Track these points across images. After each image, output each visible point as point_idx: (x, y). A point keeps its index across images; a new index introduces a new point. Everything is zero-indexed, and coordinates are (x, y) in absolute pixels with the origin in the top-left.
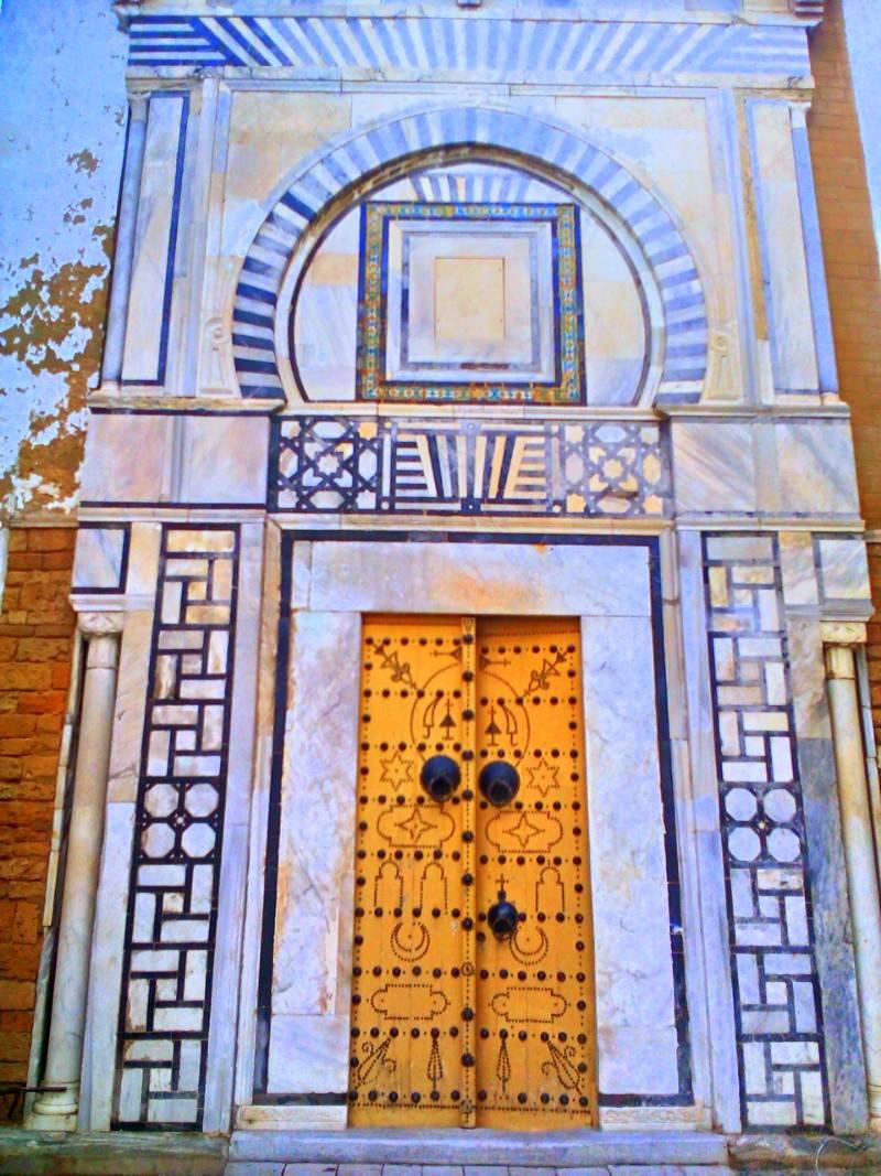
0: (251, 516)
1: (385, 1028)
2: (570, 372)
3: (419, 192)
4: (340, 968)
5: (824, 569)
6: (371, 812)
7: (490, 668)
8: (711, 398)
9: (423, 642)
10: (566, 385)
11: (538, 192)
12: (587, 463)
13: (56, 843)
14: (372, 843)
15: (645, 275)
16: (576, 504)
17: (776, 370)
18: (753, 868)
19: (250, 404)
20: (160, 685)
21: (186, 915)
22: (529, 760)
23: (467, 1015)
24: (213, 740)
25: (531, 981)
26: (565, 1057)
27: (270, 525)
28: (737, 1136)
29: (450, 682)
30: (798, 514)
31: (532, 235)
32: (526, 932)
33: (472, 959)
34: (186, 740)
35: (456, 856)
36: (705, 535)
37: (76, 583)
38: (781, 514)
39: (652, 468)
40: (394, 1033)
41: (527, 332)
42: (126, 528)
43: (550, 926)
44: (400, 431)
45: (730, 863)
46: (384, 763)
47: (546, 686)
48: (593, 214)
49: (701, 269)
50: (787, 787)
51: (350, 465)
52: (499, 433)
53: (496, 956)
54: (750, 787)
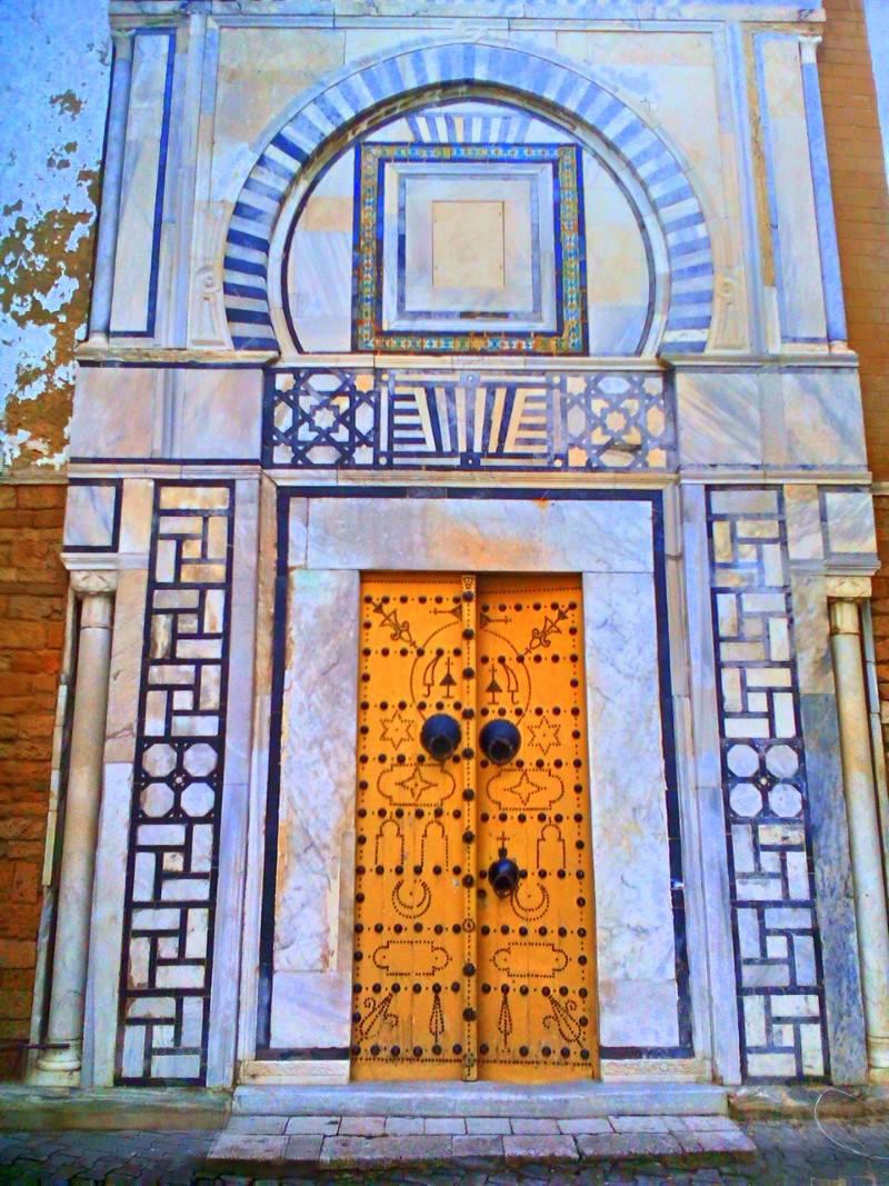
0: (245, 472)
1: (387, 983)
2: (572, 320)
3: (416, 133)
4: (342, 923)
5: (830, 523)
6: (371, 772)
7: (491, 626)
8: (715, 347)
9: (423, 600)
10: (568, 335)
11: (539, 132)
12: (590, 416)
13: (54, 803)
14: (373, 801)
15: (650, 221)
16: (577, 458)
17: (783, 316)
18: (754, 824)
19: (243, 356)
20: (156, 645)
21: (186, 873)
22: (530, 718)
23: (468, 971)
24: (211, 700)
25: (533, 936)
26: (567, 1011)
27: (266, 481)
28: (737, 1087)
29: (449, 640)
30: (804, 467)
31: (532, 177)
32: (527, 889)
33: (473, 915)
34: (183, 700)
35: (457, 814)
36: (709, 488)
37: (67, 542)
38: (787, 467)
39: (656, 420)
40: (396, 988)
41: (527, 278)
42: (118, 484)
43: (551, 881)
44: (397, 384)
45: (731, 819)
46: (383, 722)
47: (548, 643)
48: (596, 155)
49: (707, 213)
50: (789, 742)
51: (347, 419)
52: (499, 385)
53: (498, 913)
54: (752, 743)
